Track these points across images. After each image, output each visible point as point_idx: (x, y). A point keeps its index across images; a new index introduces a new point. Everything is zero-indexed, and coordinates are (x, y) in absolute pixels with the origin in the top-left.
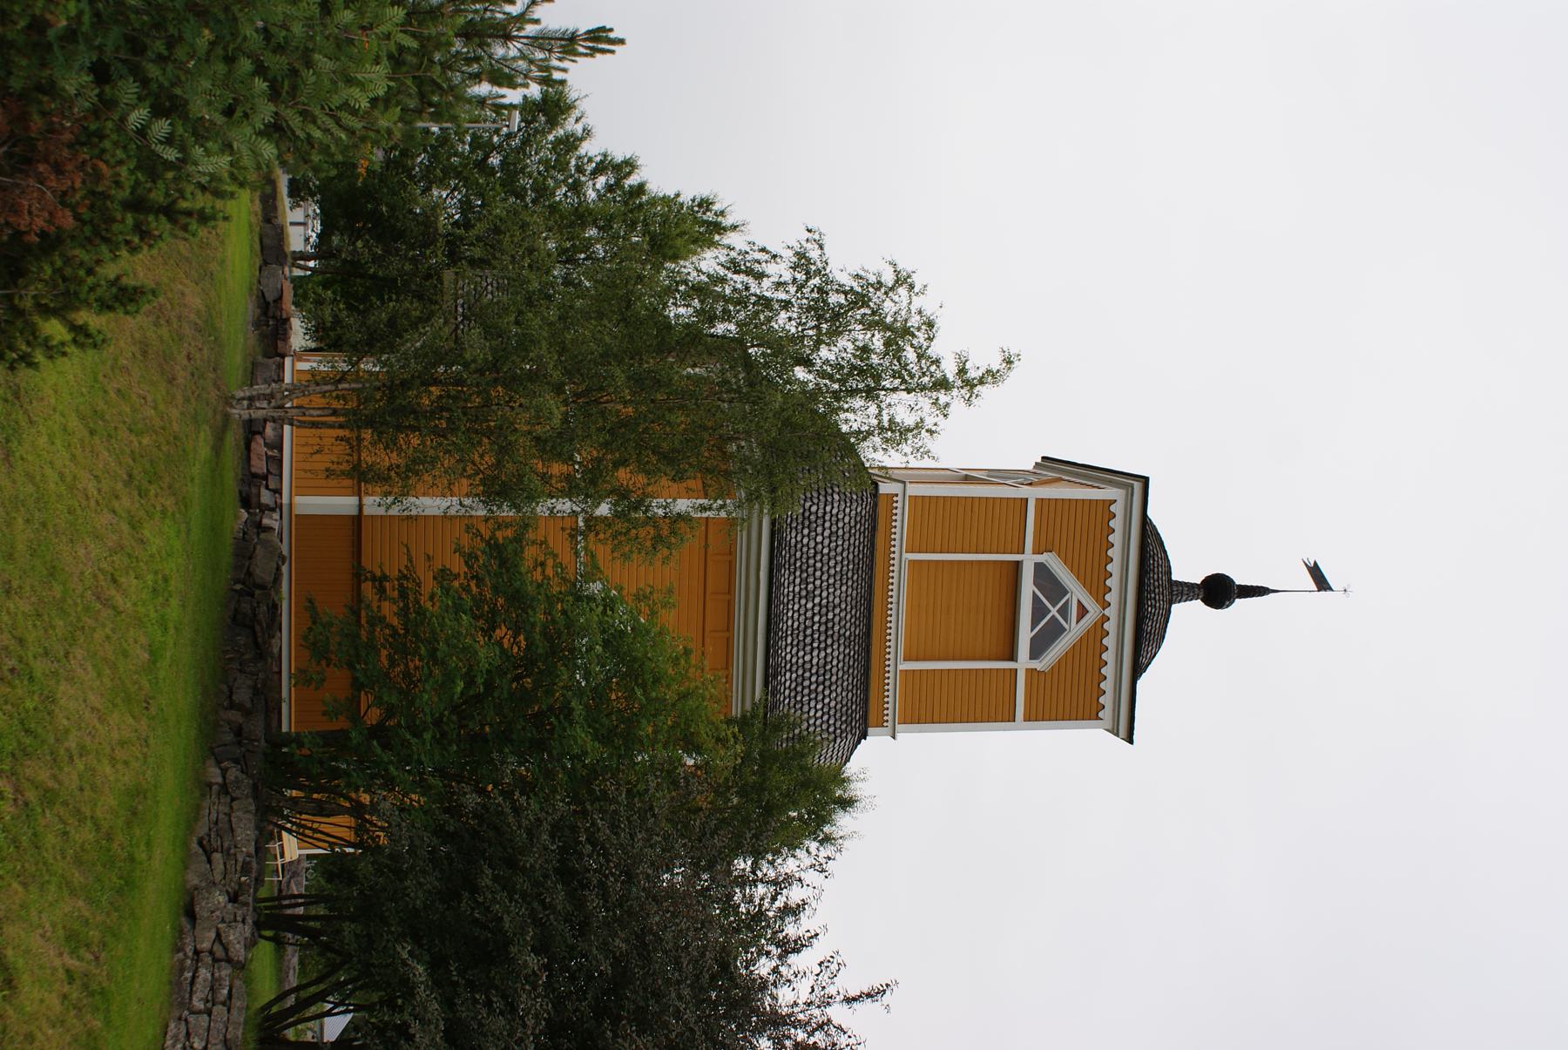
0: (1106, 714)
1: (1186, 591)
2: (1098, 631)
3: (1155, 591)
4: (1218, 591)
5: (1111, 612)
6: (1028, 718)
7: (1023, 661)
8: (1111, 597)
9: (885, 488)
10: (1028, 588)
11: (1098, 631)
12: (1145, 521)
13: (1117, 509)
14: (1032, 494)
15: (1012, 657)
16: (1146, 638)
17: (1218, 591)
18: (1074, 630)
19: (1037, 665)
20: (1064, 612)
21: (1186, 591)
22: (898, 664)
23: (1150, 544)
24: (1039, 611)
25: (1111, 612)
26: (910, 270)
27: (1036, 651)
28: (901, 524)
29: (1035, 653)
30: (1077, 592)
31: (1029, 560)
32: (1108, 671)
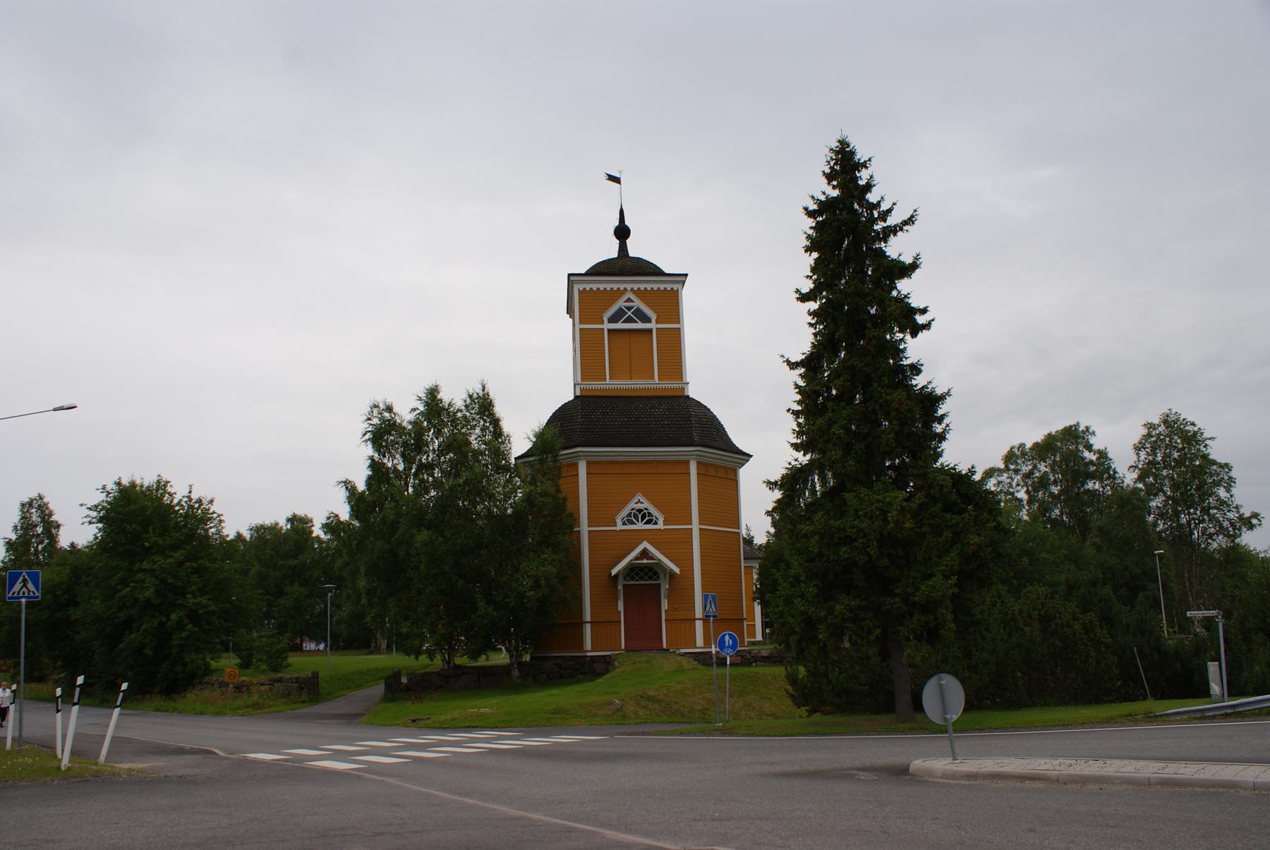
0: (675, 287)
1: (623, 249)
2: (638, 293)
3: (624, 266)
4: (622, 232)
5: (629, 287)
6: (678, 322)
7: (652, 326)
8: (622, 287)
9: (578, 394)
10: (620, 326)
11: (638, 293)
12: (588, 273)
13: (581, 287)
14: (578, 326)
15: (651, 331)
16: (646, 269)
17: (622, 232)
18: (637, 303)
19: (654, 320)
20: (629, 308)
21: (623, 249)
22: (654, 383)
23: (601, 270)
24: (629, 320)
25: (629, 287)
26: (791, 417)
27: (648, 320)
28: (596, 386)
29: (649, 321)
30: (621, 303)
31: (607, 326)
32: (662, 287)
